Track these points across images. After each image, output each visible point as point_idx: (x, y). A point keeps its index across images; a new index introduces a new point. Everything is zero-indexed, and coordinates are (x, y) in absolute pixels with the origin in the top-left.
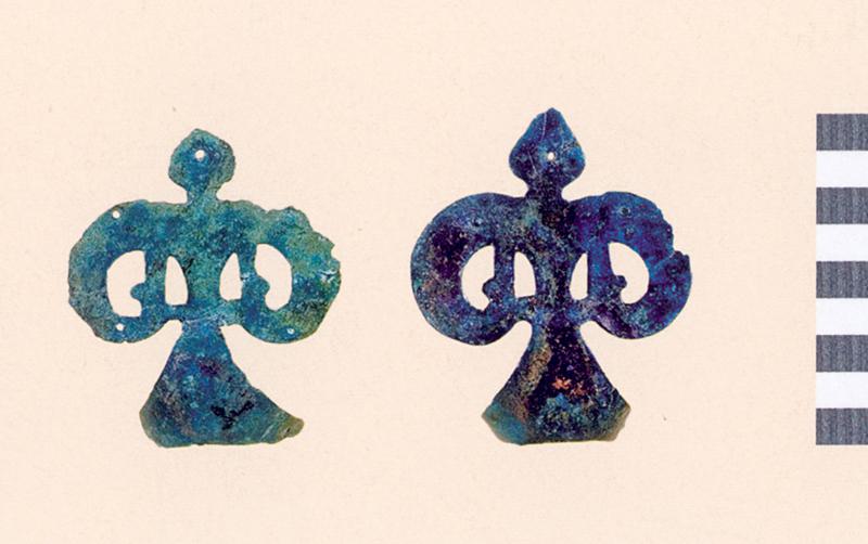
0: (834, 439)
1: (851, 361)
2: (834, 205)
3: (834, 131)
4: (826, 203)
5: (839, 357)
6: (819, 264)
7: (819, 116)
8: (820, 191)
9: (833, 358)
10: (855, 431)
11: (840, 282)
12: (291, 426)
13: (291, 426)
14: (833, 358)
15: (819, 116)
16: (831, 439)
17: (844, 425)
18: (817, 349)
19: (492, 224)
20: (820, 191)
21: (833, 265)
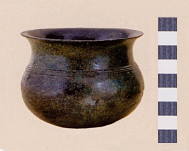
0: (165, 57)
1: (171, 84)
2: (164, 108)
3: (165, 52)
4: (161, 51)
5: (166, 110)
6: (159, 46)
7: (159, 18)
8: (159, 75)
9: (164, 54)
10: (172, 82)
11: (167, 54)
12: (22, 34)
13: (22, 34)
14: (164, 54)
15: (159, 18)
16: (164, 57)
17: (168, 52)
18: (159, 26)
20: (159, 75)
21: (164, 47)
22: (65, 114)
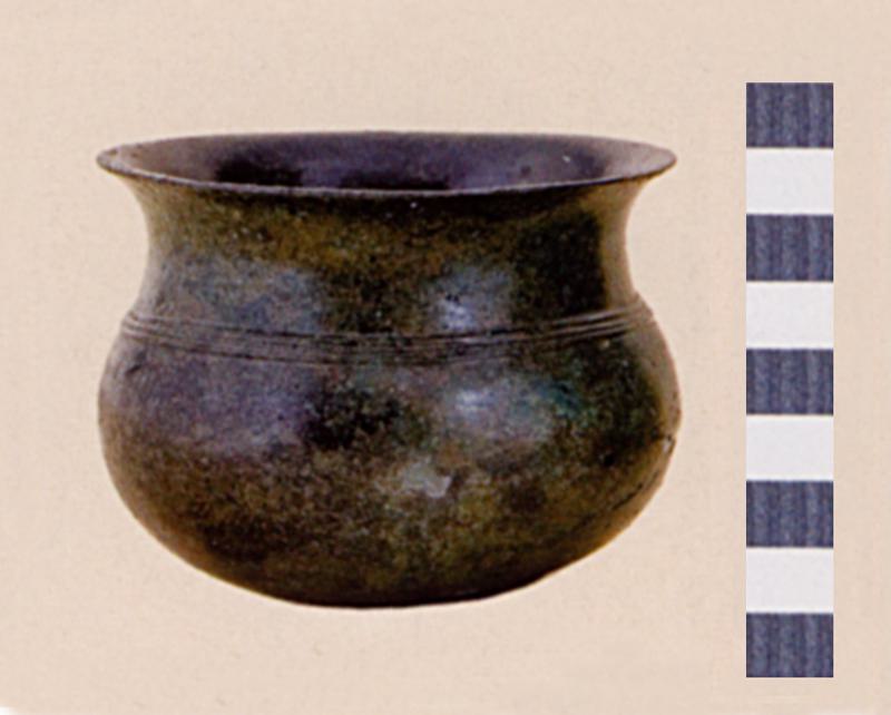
0: (776, 271)
1: (806, 395)
2: (774, 513)
3: (776, 248)
4: (761, 243)
5: (783, 521)
6: (751, 219)
7: (751, 87)
8: (751, 355)
9: (774, 257)
10: (813, 390)
11: (787, 255)
12: (106, 162)
13: (106, 162)
14: (774, 257)
15: (751, 87)
16: (771, 269)
18: (749, 124)
19: (304, 539)
20: (751, 355)
21: (774, 221)
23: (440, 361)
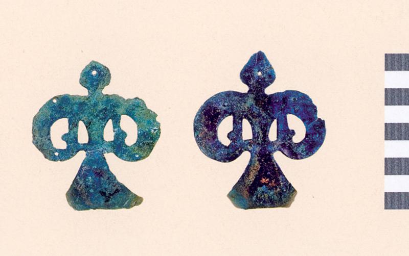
0: (393, 206)
1: (401, 170)
2: (393, 97)
3: (393, 62)
4: (389, 95)
5: (395, 168)
6: (386, 124)
7: (386, 55)
8: (386, 90)
9: (392, 169)
10: (403, 203)
11: (396, 132)
12: (137, 200)
13: (137, 200)
14: (392, 169)
15: (386, 55)
16: (391, 206)
18: (385, 164)
20: (386, 90)
21: (393, 125)
22: (232, 105)
23: (244, 96)
